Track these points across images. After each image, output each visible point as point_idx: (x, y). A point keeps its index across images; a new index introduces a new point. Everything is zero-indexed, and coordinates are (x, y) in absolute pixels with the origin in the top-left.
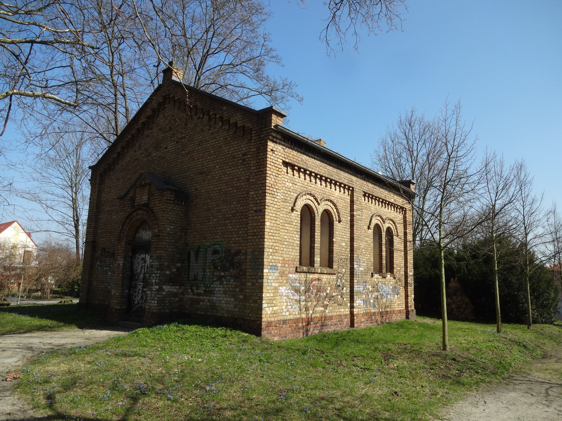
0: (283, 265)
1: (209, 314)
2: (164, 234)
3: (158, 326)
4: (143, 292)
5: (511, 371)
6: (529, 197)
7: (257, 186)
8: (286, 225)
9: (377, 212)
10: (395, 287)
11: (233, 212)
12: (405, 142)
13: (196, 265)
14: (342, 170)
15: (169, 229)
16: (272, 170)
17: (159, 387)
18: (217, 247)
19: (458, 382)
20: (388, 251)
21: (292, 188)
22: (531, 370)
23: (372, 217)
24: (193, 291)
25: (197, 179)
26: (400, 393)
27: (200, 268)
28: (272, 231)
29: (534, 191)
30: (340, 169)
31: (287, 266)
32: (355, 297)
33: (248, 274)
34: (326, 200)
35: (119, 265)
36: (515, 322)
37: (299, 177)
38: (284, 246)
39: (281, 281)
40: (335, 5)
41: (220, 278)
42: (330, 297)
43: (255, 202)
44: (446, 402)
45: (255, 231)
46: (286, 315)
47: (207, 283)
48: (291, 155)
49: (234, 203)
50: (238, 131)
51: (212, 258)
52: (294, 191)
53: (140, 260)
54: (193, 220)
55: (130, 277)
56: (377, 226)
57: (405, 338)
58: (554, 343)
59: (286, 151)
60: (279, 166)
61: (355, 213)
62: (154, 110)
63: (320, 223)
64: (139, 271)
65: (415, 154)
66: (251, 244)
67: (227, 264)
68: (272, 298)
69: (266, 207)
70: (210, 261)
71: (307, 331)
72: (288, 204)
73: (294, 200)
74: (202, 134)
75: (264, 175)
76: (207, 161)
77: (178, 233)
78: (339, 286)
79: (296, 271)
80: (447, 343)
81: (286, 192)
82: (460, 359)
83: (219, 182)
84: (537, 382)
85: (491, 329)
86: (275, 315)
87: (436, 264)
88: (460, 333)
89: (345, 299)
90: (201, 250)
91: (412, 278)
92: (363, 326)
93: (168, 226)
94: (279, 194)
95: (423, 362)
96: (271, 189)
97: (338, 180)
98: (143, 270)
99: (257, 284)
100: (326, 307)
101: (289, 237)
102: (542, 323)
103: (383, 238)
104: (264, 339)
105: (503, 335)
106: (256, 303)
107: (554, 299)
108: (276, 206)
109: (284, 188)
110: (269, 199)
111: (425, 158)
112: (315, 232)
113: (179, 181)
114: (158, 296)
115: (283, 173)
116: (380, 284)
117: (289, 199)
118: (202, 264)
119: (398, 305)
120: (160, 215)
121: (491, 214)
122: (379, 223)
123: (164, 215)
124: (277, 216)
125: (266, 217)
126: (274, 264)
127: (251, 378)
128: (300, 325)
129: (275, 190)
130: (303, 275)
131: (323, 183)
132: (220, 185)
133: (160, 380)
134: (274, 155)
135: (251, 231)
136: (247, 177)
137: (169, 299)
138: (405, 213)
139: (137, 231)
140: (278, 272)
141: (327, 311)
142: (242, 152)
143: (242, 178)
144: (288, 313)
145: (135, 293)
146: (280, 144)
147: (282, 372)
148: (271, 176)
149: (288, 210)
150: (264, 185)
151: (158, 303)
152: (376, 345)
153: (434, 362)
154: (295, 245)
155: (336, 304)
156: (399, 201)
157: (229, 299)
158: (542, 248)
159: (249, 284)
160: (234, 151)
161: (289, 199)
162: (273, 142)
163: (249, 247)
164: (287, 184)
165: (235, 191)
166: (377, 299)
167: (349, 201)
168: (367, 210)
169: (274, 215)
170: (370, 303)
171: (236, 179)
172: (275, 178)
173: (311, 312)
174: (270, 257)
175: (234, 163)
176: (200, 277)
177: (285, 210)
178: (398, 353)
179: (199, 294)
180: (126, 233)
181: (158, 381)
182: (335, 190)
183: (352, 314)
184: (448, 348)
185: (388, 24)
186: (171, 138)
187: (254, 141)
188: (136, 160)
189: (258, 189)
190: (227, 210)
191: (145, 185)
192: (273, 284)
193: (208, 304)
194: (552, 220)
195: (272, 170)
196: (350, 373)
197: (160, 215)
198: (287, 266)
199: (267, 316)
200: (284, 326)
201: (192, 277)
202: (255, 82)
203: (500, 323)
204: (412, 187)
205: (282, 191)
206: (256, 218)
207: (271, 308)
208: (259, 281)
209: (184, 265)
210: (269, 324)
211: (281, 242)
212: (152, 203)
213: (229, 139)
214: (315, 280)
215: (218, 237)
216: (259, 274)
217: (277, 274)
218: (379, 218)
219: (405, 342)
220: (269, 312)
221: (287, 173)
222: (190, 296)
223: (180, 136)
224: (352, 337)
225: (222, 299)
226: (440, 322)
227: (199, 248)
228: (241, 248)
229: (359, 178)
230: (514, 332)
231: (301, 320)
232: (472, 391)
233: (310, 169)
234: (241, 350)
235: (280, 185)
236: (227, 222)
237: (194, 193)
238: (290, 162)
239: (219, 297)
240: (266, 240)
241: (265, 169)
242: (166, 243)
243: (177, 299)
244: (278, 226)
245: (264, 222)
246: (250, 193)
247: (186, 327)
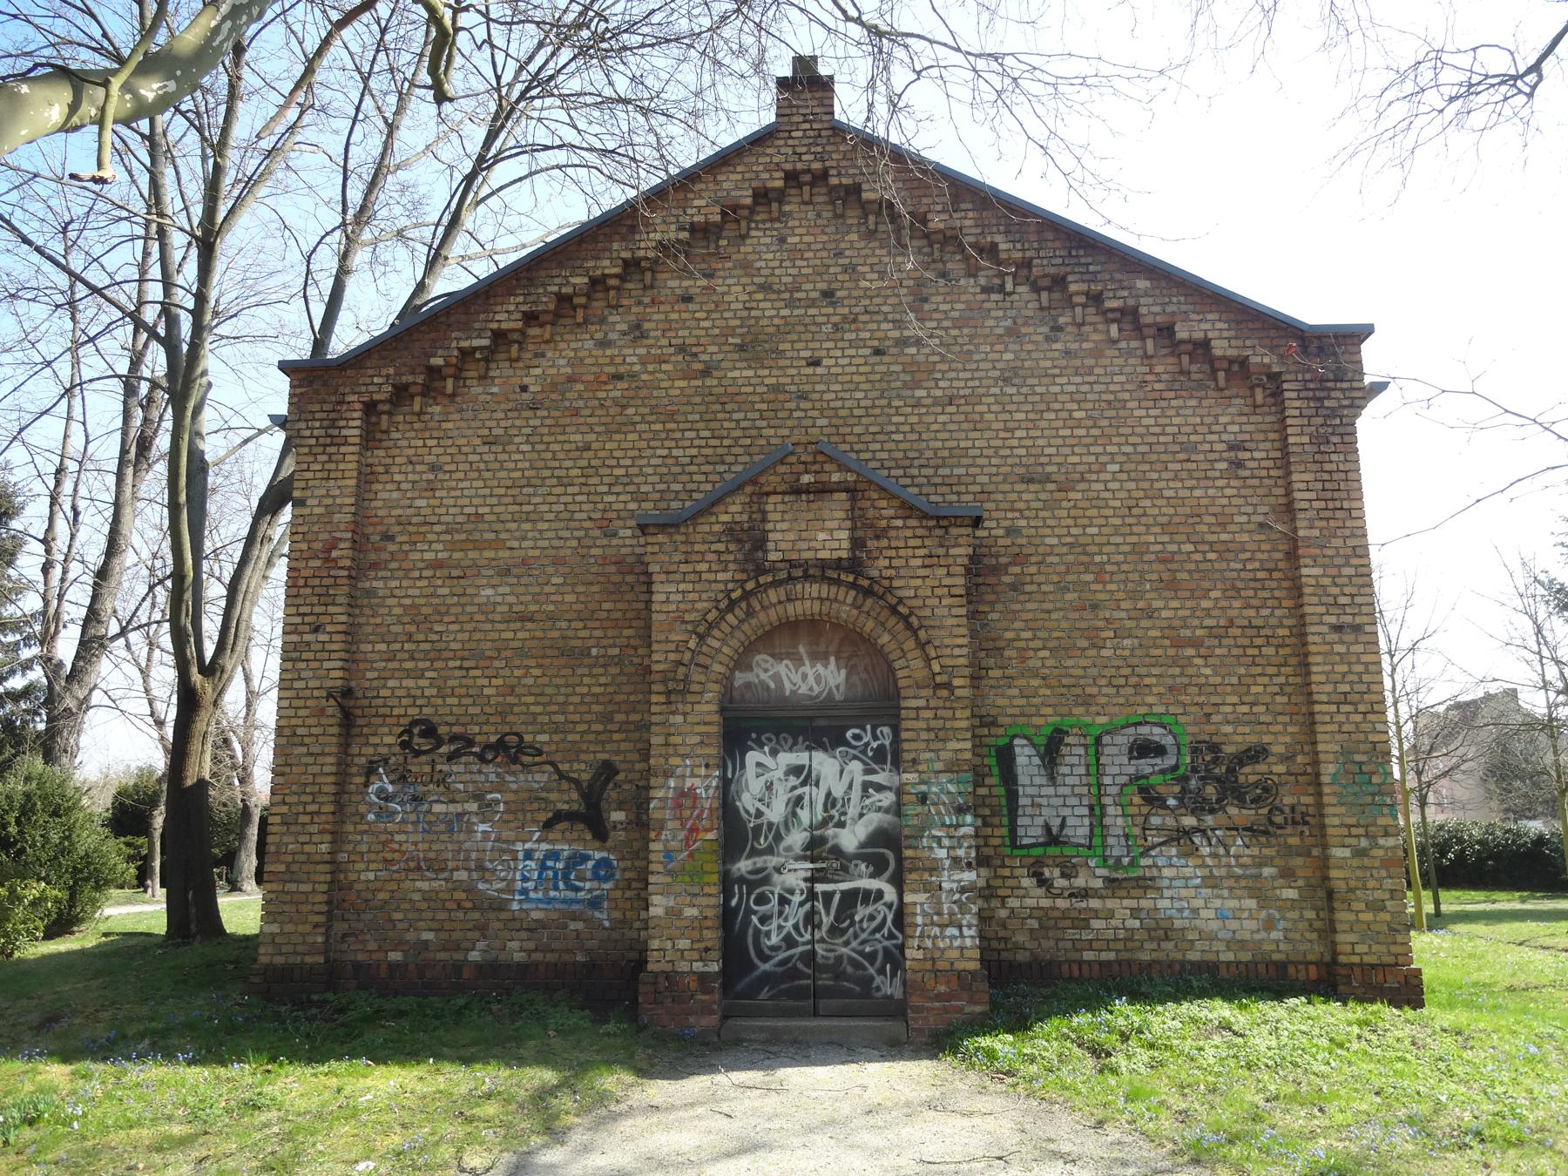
1: (1145, 957)
11: (1208, 622)
24: (1043, 882)
41: (1180, 836)
51: (1132, 770)
54: (1009, 635)
98: (804, 815)
145: (762, 900)
165: (1211, 556)
176: (1079, 829)
179: (1084, 894)
188: (618, 377)
201: (1030, 831)
206: (1340, 649)
222: (1030, 902)
225: (1199, 903)
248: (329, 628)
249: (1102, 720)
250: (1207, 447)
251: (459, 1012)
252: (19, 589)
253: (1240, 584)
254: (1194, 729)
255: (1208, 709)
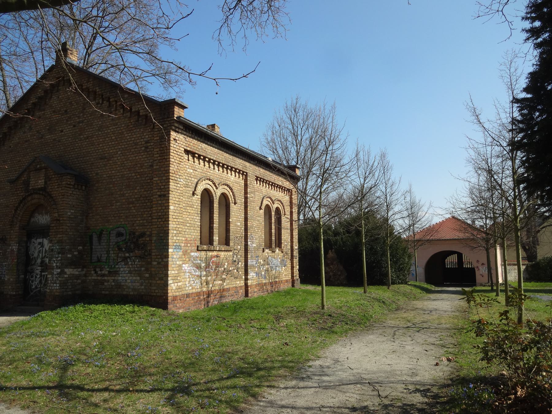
0: (186, 245)
1: (115, 293)
2: (65, 219)
3: (63, 308)
4: (41, 275)
5: (372, 321)
6: (390, 180)
7: (160, 173)
8: (188, 208)
9: (268, 193)
10: (283, 260)
11: (136, 196)
12: (290, 127)
13: (99, 247)
14: (237, 157)
15: (69, 214)
16: (175, 158)
17: (83, 358)
18: (121, 230)
19: (333, 332)
20: (277, 229)
21: (193, 174)
22: (386, 319)
23: (263, 198)
24: (96, 272)
25: (98, 164)
26: (289, 344)
27: (103, 250)
28: (176, 214)
29: (394, 176)
30: (235, 156)
31: (189, 245)
32: (249, 270)
33: (154, 254)
34: (223, 185)
35: (12, 250)
36: (379, 285)
37: (199, 164)
38: (186, 227)
39: (184, 259)
40: (228, 10)
41: (125, 259)
42: (227, 272)
43: (159, 187)
44: (324, 346)
45: (160, 214)
46: (189, 290)
47: (111, 264)
48: (191, 144)
49: (138, 188)
50: (140, 119)
51: (116, 241)
52: (195, 177)
53: (37, 245)
54: (94, 204)
55: (26, 261)
56: (267, 206)
57: (291, 303)
58: (406, 299)
59: (187, 140)
60: (181, 154)
61: (248, 196)
62: (46, 92)
63: (218, 206)
64: (36, 255)
65: (299, 138)
66: (156, 226)
67: (132, 246)
68: (177, 275)
69: (170, 192)
70: (114, 243)
71: (208, 302)
72: (189, 189)
73: (194, 185)
74: (101, 120)
75: (168, 163)
76: (108, 146)
77: (79, 217)
78: (235, 261)
79: (198, 250)
80: (325, 303)
81: (187, 178)
82: (334, 315)
83: (122, 168)
84: (390, 327)
85: (359, 290)
86: (179, 290)
87: (316, 239)
88: (335, 295)
89: (240, 273)
90: (104, 233)
91: (297, 251)
92: (256, 295)
93: (69, 211)
94: (182, 180)
95: (307, 319)
96: (174, 175)
97: (234, 166)
98: (41, 255)
99: (163, 263)
100: (223, 280)
101: (191, 219)
102: (399, 283)
103: (273, 217)
104: (170, 312)
105: (368, 295)
106: (162, 280)
107: (407, 264)
108: (179, 191)
109: (186, 174)
110: (172, 185)
111: (308, 142)
112: (213, 214)
113: (78, 165)
114: (60, 279)
115: (185, 160)
116: (270, 258)
117: (190, 184)
118: (106, 247)
119: (285, 275)
120: (60, 200)
121: (362, 194)
122: (269, 204)
123: (65, 199)
124: (180, 200)
125: (170, 201)
126: (178, 244)
127: (166, 344)
128: (202, 297)
129: (177, 176)
130: (203, 253)
131: (221, 169)
132: (123, 170)
133: (82, 352)
134: (176, 144)
135: (156, 214)
136: (150, 164)
137: (71, 281)
138: (292, 195)
139: (32, 215)
140: (182, 251)
141: (225, 284)
142: (145, 139)
143: (145, 164)
144: (190, 288)
145: (32, 277)
146: (182, 133)
147: (191, 336)
148: (174, 164)
149: (189, 195)
150: (168, 172)
151: (60, 286)
152: (269, 309)
153: (314, 319)
154: (196, 226)
155: (233, 278)
156: (287, 184)
157: (134, 278)
158: (401, 222)
159: (155, 263)
160: (136, 138)
161: (190, 184)
162: (176, 131)
163: (153, 229)
164: (189, 170)
165: (138, 176)
166: (268, 271)
167: (243, 185)
168: (260, 193)
169: (177, 200)
170: (262, 275)
171: (139, 165)
172: (178, 165)
173: (211, 285)
174: (174, 238)
175: (137, 150)
176: (104, 259)
177: (187, 194)
178: (287, 314)
179: (104, 275)
180: (20, 218)
181: (80, 353)
182: (231, 175)
183: (246, 285)
184: (326, 307)
185: (274, 31)
186: (67, 121)
187: (157, 130)
188: (26, 141)
189: (162, 175)
190: (131, 194)
191: (40, 169)
192: (178, 263)
193: (113, 284)
194: (408, 199)
195: (175, 158)
196: (249, 333)
197: (60, 200)
198: (189, 245)
199: (173, 291)
200: (188, 299)
201: (95, 258)
202: (149, 64)
203: (366, 285)
204: (297, 170)
205: (184, 177)
206: (160, 202)
207: (176, 284)
208: (164, 260)
209: (86, 248)
210: (175, 298)
211: (184, 224)
212: (50, 187)
213: (131, 126)
214: (214, 257)
215: (122, 220)
216: (165, 254)
217: (181, 253)
218: (269, 200)
219: (292, 306)
220: (174, 288)
221: (188, 160)
222: (93, 278)
223: (78, 120)
224: (247, 305)
225: (127, 278)
226: (319, 288)
227: (102, 230)
228: (146, 230)
229: (252, 164)
230: (377, 292)
231: (202, 293)
232: (342, 337)
233: (209, 157)
234: (150, 322)
235: (182, 172)
236: (131, 206)
237: (95, 177)
238: (191, 150)
239: (125, 277)
240: (170, 222)
241: (168, 157)
242: (67, 227)
243: (79, 281)
244: (181, 209)
245: (169, 206)
246: (154, 179)
247: (92, 307)
248: (157, 196)
249: (111, 226)
250: (140, 143)
251: (346, 332)
252: (524, 188)
253: (144, 184)
254: (129, 228)
255: (134, 222)
